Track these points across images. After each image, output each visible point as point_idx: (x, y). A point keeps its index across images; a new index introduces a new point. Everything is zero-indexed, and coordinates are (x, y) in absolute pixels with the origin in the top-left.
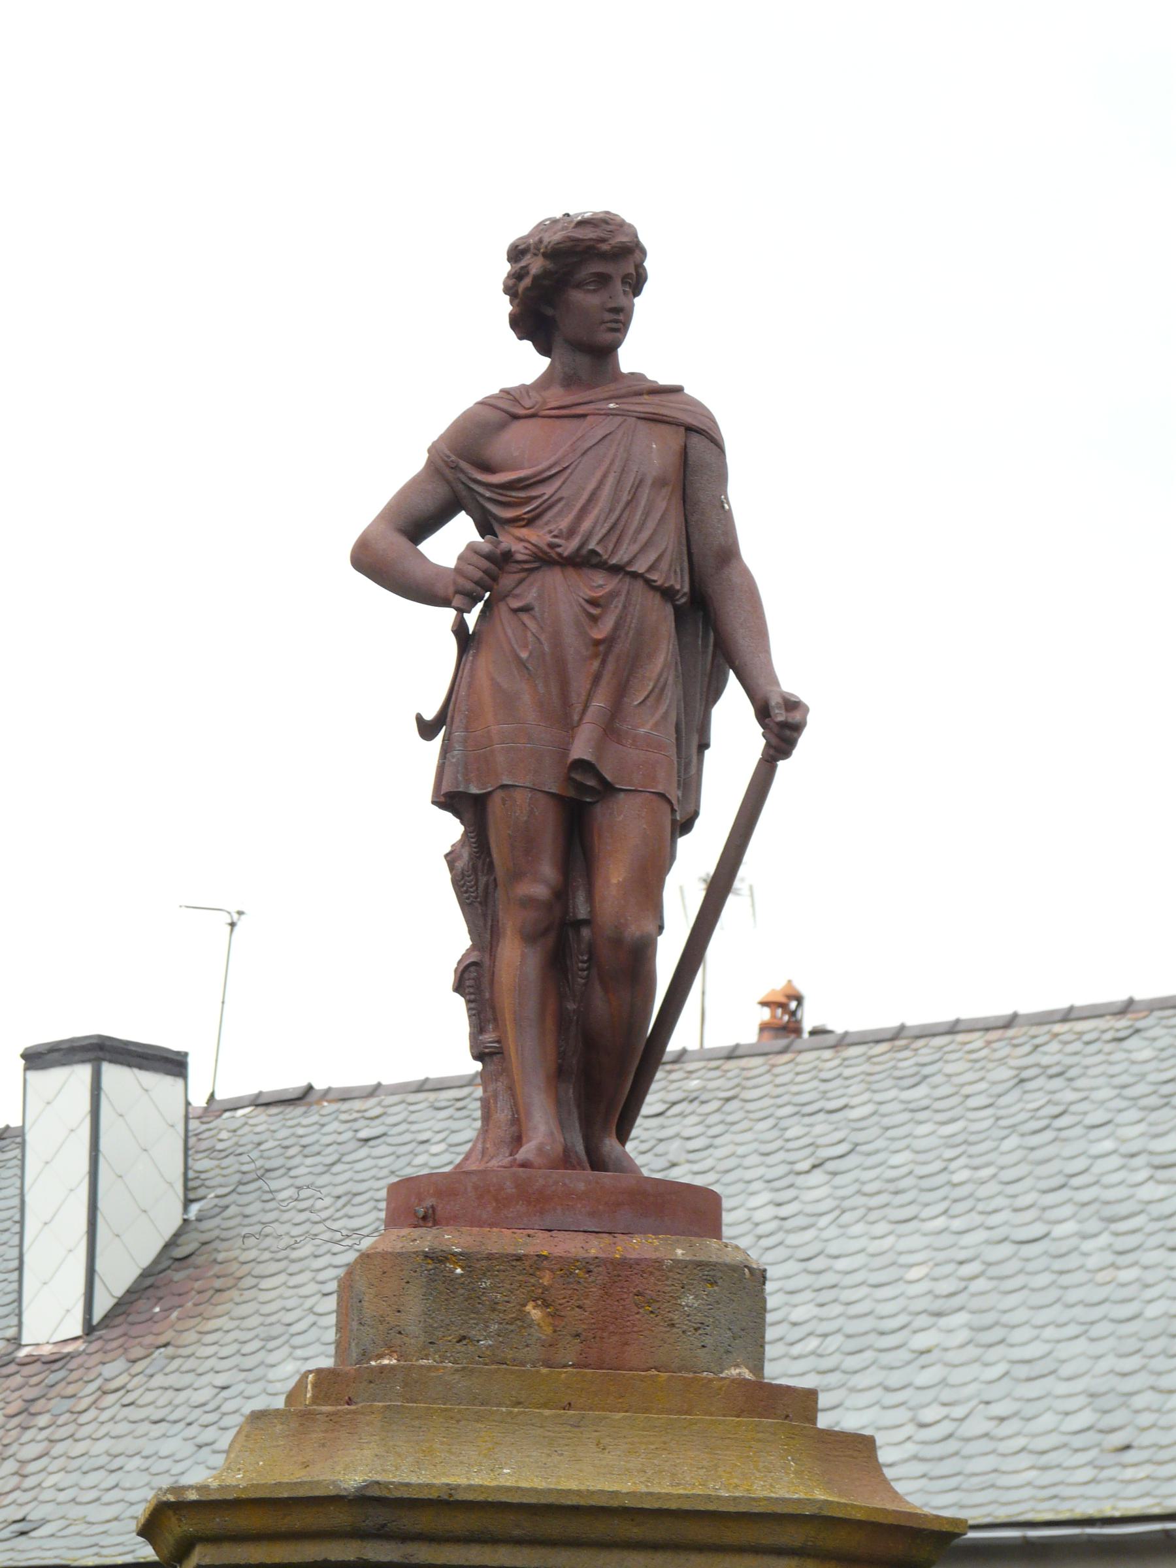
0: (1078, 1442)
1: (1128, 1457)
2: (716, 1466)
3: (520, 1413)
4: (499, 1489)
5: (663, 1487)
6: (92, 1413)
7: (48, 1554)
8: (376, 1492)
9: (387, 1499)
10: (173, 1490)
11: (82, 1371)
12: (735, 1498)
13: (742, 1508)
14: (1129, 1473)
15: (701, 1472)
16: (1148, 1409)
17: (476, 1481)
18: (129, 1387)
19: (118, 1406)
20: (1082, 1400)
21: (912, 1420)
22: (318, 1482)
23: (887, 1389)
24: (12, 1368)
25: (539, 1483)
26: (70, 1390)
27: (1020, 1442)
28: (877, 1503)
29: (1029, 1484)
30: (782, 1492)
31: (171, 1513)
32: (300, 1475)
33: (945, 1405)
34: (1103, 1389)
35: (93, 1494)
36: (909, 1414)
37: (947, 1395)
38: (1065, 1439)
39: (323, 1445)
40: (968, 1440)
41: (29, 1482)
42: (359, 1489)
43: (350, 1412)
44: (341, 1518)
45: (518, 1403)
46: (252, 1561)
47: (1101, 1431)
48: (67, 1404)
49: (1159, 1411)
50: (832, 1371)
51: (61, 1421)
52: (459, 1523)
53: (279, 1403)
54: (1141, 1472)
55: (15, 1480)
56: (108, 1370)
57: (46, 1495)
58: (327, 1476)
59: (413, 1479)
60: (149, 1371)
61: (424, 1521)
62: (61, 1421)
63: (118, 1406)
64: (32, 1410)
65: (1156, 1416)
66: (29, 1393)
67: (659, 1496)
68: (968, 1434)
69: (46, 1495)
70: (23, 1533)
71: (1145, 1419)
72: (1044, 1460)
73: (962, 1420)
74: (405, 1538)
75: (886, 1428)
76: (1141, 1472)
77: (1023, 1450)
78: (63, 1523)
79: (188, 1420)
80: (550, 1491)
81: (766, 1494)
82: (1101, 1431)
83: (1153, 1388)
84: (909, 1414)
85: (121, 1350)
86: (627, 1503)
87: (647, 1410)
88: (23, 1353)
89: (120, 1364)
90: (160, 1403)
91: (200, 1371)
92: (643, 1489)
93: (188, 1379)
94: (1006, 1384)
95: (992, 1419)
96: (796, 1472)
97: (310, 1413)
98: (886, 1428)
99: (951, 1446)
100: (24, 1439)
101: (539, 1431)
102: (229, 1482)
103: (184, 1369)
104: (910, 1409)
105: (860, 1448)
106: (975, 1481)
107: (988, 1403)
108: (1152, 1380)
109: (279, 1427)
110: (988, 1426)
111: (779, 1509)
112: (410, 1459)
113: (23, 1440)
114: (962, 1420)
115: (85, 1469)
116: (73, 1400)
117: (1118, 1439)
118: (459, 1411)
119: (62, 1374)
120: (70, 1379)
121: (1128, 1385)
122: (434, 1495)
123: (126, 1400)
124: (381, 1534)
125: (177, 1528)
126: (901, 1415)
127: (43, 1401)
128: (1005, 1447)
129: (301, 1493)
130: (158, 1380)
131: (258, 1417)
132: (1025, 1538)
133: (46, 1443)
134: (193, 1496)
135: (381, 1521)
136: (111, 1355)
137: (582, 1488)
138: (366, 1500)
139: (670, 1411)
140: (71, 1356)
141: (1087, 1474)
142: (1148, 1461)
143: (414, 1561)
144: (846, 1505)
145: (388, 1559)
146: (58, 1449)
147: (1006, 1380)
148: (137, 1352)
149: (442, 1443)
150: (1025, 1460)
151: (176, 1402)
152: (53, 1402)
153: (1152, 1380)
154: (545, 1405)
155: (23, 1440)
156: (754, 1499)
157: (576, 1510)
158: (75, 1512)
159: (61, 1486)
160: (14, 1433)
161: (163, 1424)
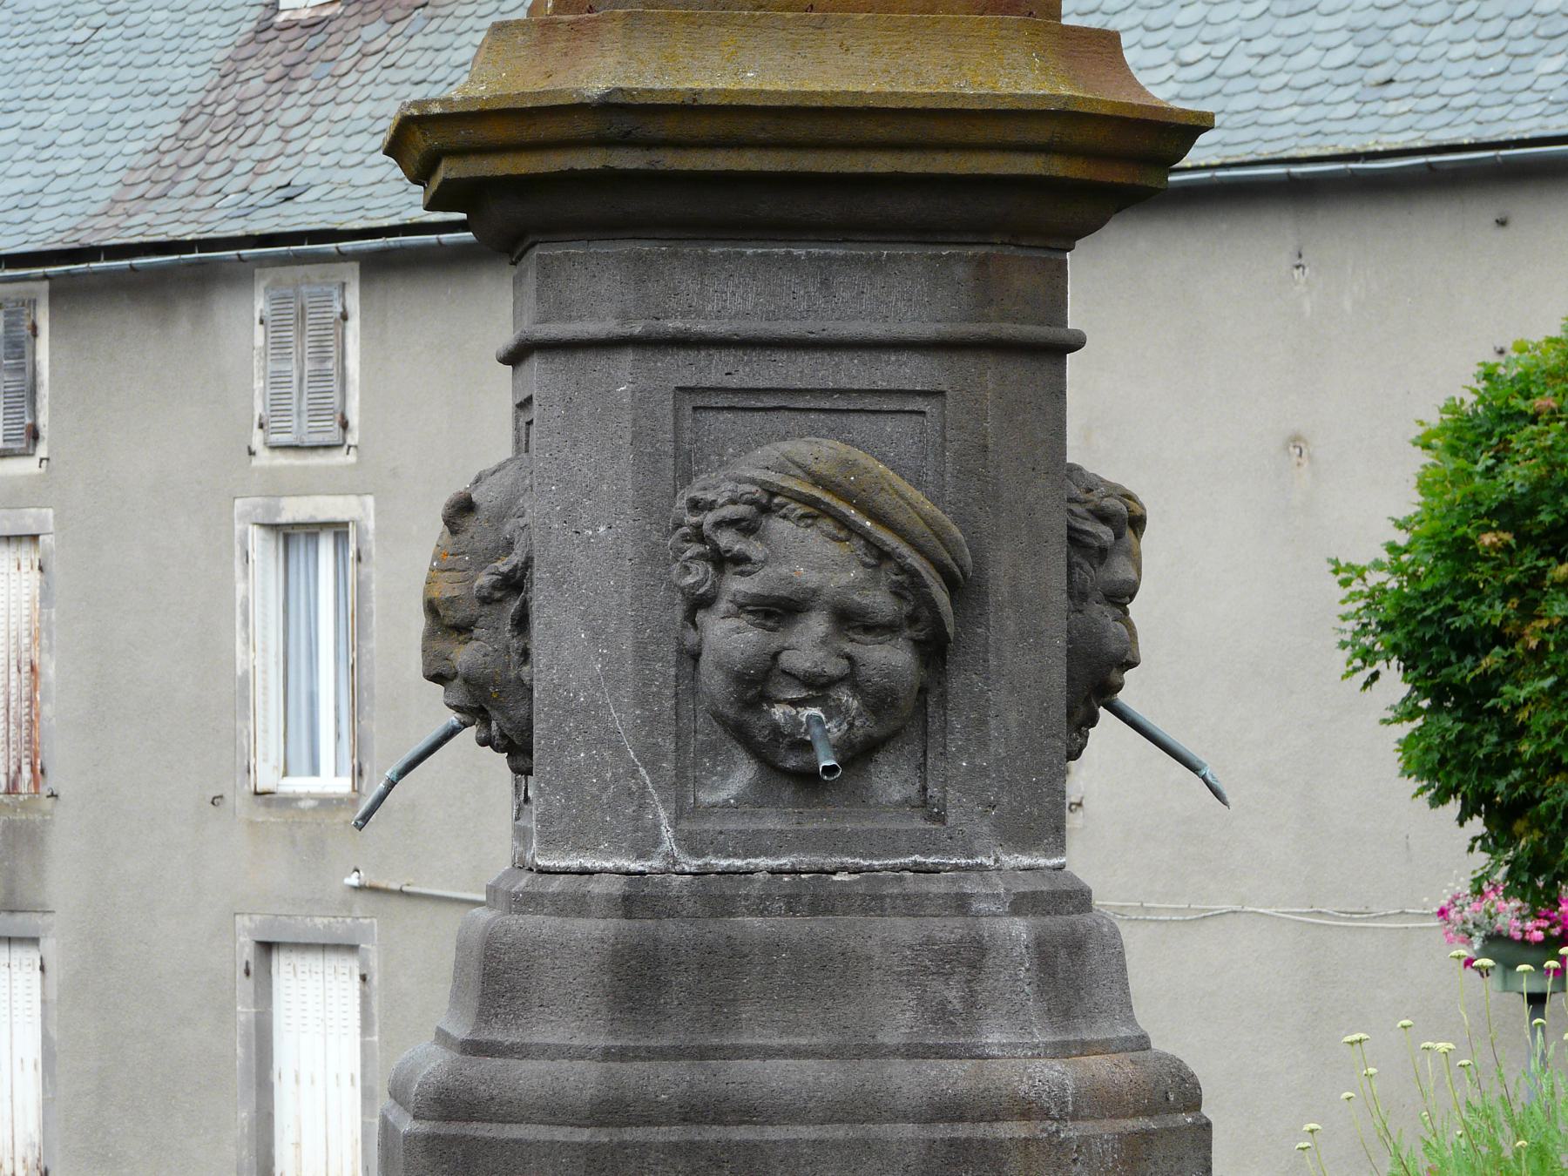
0: (1339, 77)
1: (1391, 91)
2: (961, 64)
3: (761, 17)
4: (744, 92)
5: (907, 86)
6: (353, 76)
7: (314, 218)
8: (620, 99)
9: (630, 105)
10: (416, 104)
11: (341, 34)
12: (980, 96)
13: (988, 106)
14: (1392, 107)
15: (946, 71)
16: (1409, 43)
17: (720, 86)
18: (389, 48)
19: (378, 68)
20: (1344, 35)
21: (1173, 60)
22: (561, 91)
23: (1148, 29)
24: (271, 34)
25: (783, 86)
26: (330, 54)
27: (1282, 79)
28: (1124, 98)
29: (1292, 120)
30: (1027, 89)
31: (415, 128)
32: (544, 85)
33: (1205, 43)
34: (1364, 24)
35: (357, 158)
36: (1171, 54)
37: (1207, 34)
38: (1326, 75)
39: (566, 54)
40: (1230, 78)
41: (292, 148)
42: (602, 96)
43: (590, 20)
44: (586, 127)
45: (760, 7)
46: (499, 173)
47: (1362, 66)
48: (329, 67)
49: (1420, 44)
50: (1093, 12)
51: (322, 85)
52: (704, 128)
53: (521, 14)
54: (1404, 106)
55: (279, 146)
56: (367, 33)
57: (312, 159)
58: (572, 85)
59: (657, 86)
60: (408, 32)
61: (669, 127)
62: (322, 85)
63: (378, 68)
64: (293, 75)
65: (1418, 49)
66: (290, 58)
67: (904, 96)
68: (1230, 72)
69: (312, 159)
70: (288, 199)
71: (1407, 53)
72: (1306, 96)
73: (1224, 58)
74: (650, 144)
75: (1147, 68)
76: (1404, 106)
77: (1285, 86)
78: (327, 187)
79: (450, 80)
80: (794, 93)
81: (1010, 90)
82: (1362, 66)
83: (1413, 21)
84: (1171, 54)
85: (379, 13)
86: (872, 103)
87: (890, 11)
88: (280, 18)
89: (379, 26)
90: (421, 63)
91: (460, 30)
92: (888, 89)
93: (449, 38)
94: (1267, 20)
95: (1252, 56)
96: (1040, 69)
97: (552, 22)
98: (1147, 68)
99: (1214, 84)
100: (286, 104)
101: (782, 34)
102: (472, 94)
103: (443, 28)
104: (1172, 49)
105: (1105, 44)
106: (1237, 118)
107: (1249, 40)
108: (1412, 14)
109: (521, 37)
110: (1251, 63)
111: (1023, 106)
112: (654, 65)
113: (285, 105)
114: (1224, 58)
115: (348, 132)
116: (333, 64)
117: (1380, 73)
118: (701, 16)
119: (321, 37)
120: (329, 42)
121: (1389, 19)
122: (678, 100)
123: (387, 62)
124: (626, 142)
125: (423, 142)
126: (1162, 55)
127: (303, 66)
128: (1266, 84)
129: (545, 102)
130: (418, 41)
131: (499, 28)
132: (1288, 174)
133: (307, 108)
134: (436, 109)
135: (626, 128)
136: (369, 18)
137: (827, 89)
138: (609, 107)
139: (914, 11)
140: (329, 20)
141: (1350, 109)
142: (1411, 95)
143: (660, 167)
144: (1091, 100)
145: (634, 166)
146: (320, 113)
147: (1267, 16)
148: (396, 13)
149: (685, 49)
150: (1286, 97)
151: (437, 62)
152: (314, 66)
153: (1412, 14)
154: (788, 8)
155: (285, 105)
156: (998, 96)
157: (821, 111)
158: (340, 176)
159: (325, 150)
160: (275, 99)
161: (425, 85)
